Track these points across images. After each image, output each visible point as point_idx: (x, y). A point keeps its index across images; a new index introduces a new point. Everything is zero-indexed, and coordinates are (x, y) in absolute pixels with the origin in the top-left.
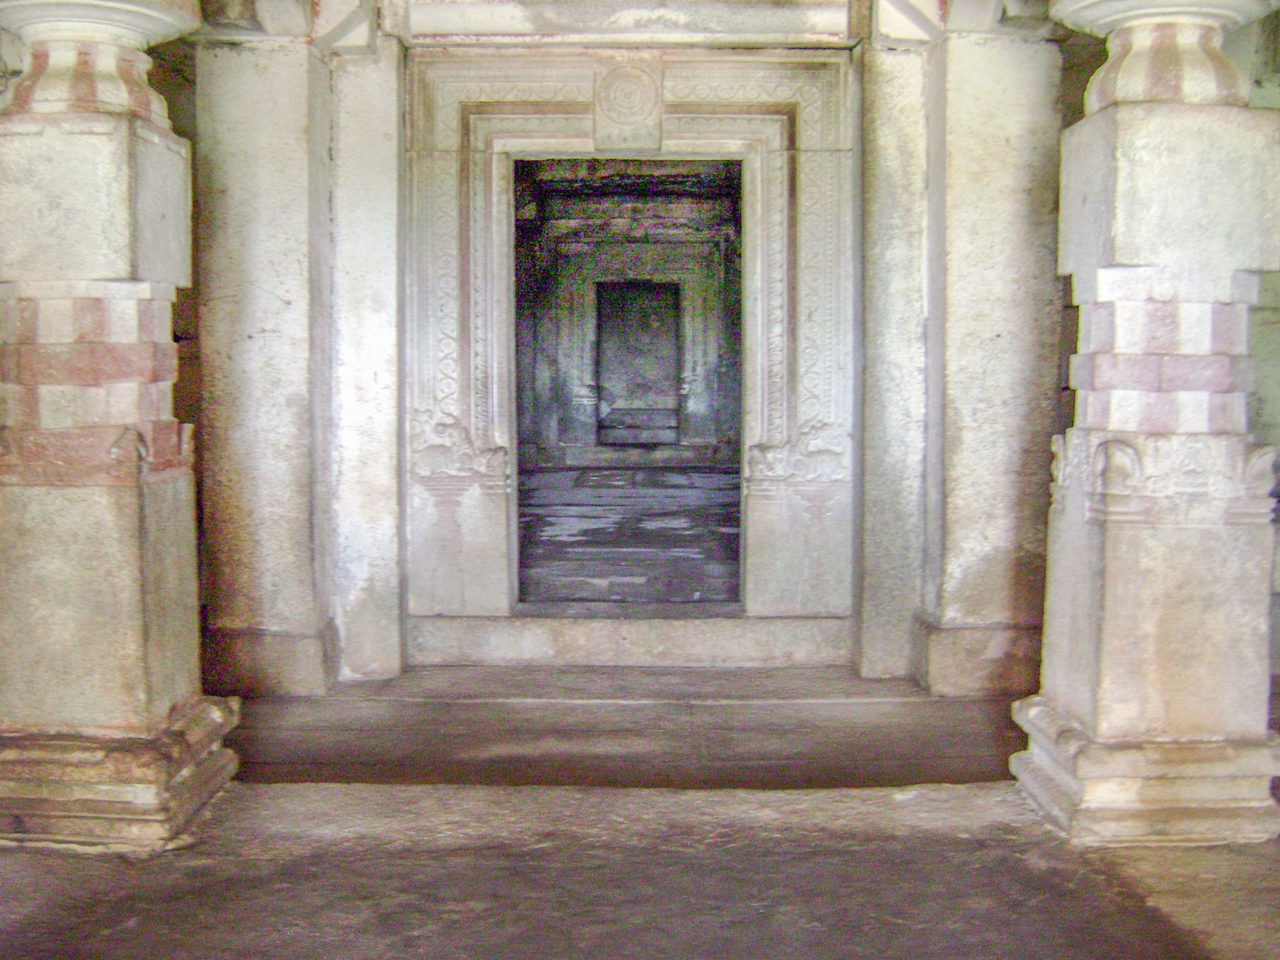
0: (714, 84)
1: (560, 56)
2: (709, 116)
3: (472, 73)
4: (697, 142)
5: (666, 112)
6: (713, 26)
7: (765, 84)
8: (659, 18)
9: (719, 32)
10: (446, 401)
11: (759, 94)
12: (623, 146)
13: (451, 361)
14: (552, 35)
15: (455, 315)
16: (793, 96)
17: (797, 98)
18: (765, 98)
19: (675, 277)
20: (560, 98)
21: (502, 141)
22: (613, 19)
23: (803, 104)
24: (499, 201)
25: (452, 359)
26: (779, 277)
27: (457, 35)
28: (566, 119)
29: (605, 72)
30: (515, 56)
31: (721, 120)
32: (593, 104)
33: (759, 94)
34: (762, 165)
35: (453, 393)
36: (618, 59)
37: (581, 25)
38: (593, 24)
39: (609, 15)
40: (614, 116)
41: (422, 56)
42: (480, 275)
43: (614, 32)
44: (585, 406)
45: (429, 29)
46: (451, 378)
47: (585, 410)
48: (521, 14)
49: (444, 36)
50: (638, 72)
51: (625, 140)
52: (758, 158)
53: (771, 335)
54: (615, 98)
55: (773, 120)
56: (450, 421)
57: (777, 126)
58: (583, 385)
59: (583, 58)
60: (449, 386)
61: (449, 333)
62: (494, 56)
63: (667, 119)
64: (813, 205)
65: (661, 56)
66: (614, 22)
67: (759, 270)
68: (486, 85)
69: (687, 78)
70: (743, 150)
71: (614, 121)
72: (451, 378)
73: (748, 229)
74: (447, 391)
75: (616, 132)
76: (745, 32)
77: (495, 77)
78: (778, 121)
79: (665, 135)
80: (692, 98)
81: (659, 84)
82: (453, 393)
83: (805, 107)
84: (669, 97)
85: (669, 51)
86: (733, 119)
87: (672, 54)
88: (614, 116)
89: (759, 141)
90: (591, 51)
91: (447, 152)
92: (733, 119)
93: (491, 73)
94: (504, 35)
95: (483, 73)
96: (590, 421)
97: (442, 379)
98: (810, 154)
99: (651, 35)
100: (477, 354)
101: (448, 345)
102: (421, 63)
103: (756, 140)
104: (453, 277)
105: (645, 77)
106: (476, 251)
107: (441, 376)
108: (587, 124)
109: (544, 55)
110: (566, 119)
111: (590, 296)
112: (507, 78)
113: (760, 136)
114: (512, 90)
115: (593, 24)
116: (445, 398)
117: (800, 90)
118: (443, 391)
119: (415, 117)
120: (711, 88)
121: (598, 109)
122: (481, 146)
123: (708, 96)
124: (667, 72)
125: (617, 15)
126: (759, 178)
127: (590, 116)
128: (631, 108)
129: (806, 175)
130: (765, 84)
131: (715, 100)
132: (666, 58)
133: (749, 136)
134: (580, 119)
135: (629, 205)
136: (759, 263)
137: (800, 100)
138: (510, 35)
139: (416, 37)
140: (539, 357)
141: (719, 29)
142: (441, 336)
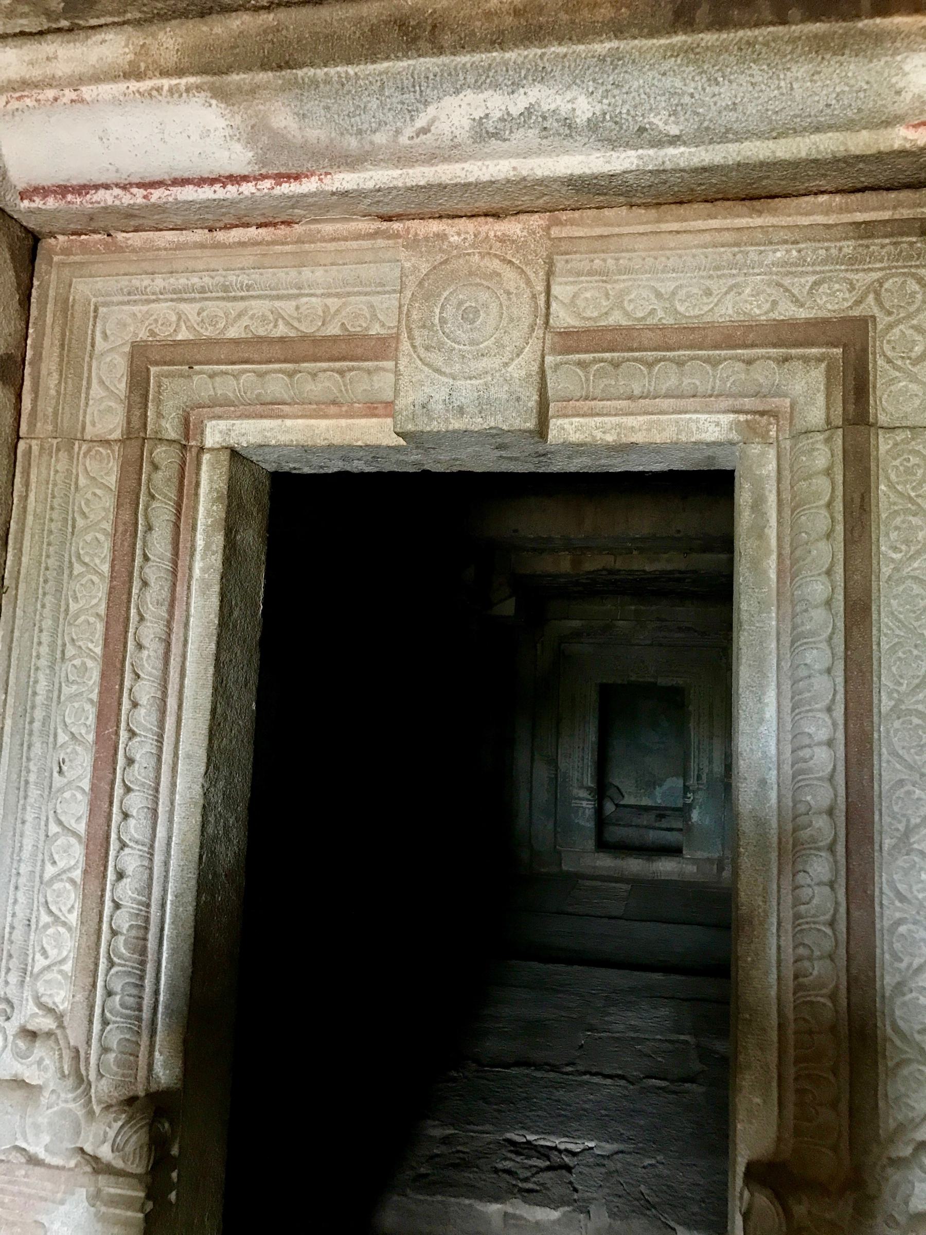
0: (666, 288)
1: (334, 239)
2: (650, 355)
3: (159, 282)
4: (630, 421)
5: (554, 351)
6: (660, 122)
7: (787, 281)
8: (529, 111)
9: (674, 141)
10: (48, 976)
11: (775, 303)
12: (456, 424)
13: (68, 886)
14: (297, 177)
15: (86, 785)
16: (858, 303)
17: (870, 306)
18: (787, 311)
19: (680, 682)
20: (333, 329)
21: (223, 424)
22: (420, 123)
23: (883, 320)
24: (207, 547)
25: (72, 881)
26: (823, 734)
27: (107, 187)
28: (341, 373)
29: (424, 268)
30: (242, 244)
31: (680, 363)
32: (397, 338)
33: (775, 303)
34: (779, 471)
35: (63, 961)
36: (454, 239)
37: (352, 143)
38: (380, 138)
39: (412, 114)
40: (437, 359)
41: (66, 251)
42: (144, 700)
43: (432, 157)
44: (585, 808)
45: (47, 176)
46: (64, 924)
47: (584, 813)
48: (222, 123)
49: (82, 189)
50: (496, 264)
51: (461, 410)
52: (772, 453)
53: (801, 878)
54: (443, 321)
55: (806, 359)
56: (46, 1023)
57: (818, 374)
58: (581, 787)
59: (381, 242)
60: (58, 942)
61: (73, 825)
62: (202, 246)
63: (557, 367)
64: (912, 558)
65: (548, 228)
66: (425, 131)
67: (770, 712)
68: (190, 309)
69: (604, 274)
70: (734, 436)
71: (438, 371)
72: (64, 924)
73: (744, 616)
74: (53, 953)
75: (441, 395)
76: (739, 138)
77: (203, 290)
78: (819, 360)
79: (553, 408)
80: (616, 318)
81: (540, 287)
82: (63, 961)
83: (890, 327)
84: (563, 317)
85: (564, 216)
86: (707, 360)
87: (572, 222)
88: (437, 359)
89: (773, 414)
90: (396, 226)
91: (106, 443)
92: (707, 360)
93: (195, 280)
94: (201, 182)
95: (182, 281)
96: (588, 825)
97: (47, 926)
98: (900, 436)
99: (514, 162)
100: (120, 875)
101: (66, 850)
102: (63, 264)
103: (762, 413)
104: (91, 701)
105: (509, 274)
106: (140, 646)
107: (45, 918)
108: (383, 384)
109: (299, 241)
110: (341, 373)
111: (593, 697)
112: (226, 293)
113: (773, 403)
114: (240, 315)
115: (380, 138)
116: (48, 968)
117: (876, 289)
118: (44, 953)
119: (44, 372)
120: (659, 295)
121: (405, 346)
122: (171, 430)
123: (653, 312)
124: (560, 262)
125: (431, 110)
126: (772, 498)
127: (390, 364)
128: (473, 342)
129: (891, 486)
130: (787, 281)
131: (669, 321)
132: (555, 232)
133: (748, 403)
134: (369, 372)
135: (633, 608)
136: (771, 696)
137: (876, 311)
138: (212, 181)
139: (23, 195)
140: (537, 756)
141: (674, 130)
142: (54, 828)
